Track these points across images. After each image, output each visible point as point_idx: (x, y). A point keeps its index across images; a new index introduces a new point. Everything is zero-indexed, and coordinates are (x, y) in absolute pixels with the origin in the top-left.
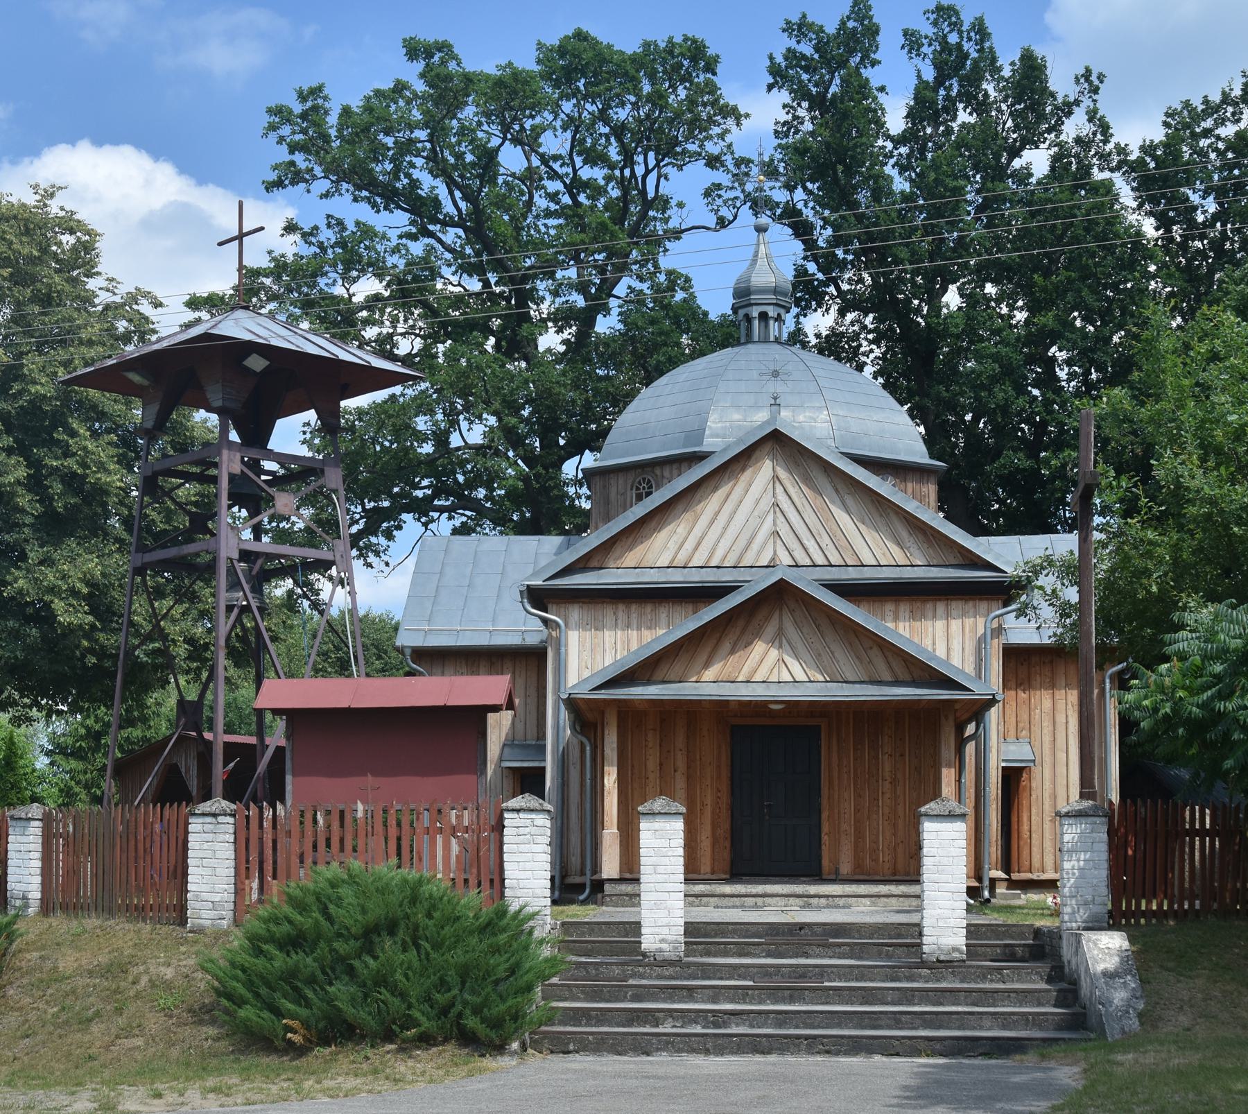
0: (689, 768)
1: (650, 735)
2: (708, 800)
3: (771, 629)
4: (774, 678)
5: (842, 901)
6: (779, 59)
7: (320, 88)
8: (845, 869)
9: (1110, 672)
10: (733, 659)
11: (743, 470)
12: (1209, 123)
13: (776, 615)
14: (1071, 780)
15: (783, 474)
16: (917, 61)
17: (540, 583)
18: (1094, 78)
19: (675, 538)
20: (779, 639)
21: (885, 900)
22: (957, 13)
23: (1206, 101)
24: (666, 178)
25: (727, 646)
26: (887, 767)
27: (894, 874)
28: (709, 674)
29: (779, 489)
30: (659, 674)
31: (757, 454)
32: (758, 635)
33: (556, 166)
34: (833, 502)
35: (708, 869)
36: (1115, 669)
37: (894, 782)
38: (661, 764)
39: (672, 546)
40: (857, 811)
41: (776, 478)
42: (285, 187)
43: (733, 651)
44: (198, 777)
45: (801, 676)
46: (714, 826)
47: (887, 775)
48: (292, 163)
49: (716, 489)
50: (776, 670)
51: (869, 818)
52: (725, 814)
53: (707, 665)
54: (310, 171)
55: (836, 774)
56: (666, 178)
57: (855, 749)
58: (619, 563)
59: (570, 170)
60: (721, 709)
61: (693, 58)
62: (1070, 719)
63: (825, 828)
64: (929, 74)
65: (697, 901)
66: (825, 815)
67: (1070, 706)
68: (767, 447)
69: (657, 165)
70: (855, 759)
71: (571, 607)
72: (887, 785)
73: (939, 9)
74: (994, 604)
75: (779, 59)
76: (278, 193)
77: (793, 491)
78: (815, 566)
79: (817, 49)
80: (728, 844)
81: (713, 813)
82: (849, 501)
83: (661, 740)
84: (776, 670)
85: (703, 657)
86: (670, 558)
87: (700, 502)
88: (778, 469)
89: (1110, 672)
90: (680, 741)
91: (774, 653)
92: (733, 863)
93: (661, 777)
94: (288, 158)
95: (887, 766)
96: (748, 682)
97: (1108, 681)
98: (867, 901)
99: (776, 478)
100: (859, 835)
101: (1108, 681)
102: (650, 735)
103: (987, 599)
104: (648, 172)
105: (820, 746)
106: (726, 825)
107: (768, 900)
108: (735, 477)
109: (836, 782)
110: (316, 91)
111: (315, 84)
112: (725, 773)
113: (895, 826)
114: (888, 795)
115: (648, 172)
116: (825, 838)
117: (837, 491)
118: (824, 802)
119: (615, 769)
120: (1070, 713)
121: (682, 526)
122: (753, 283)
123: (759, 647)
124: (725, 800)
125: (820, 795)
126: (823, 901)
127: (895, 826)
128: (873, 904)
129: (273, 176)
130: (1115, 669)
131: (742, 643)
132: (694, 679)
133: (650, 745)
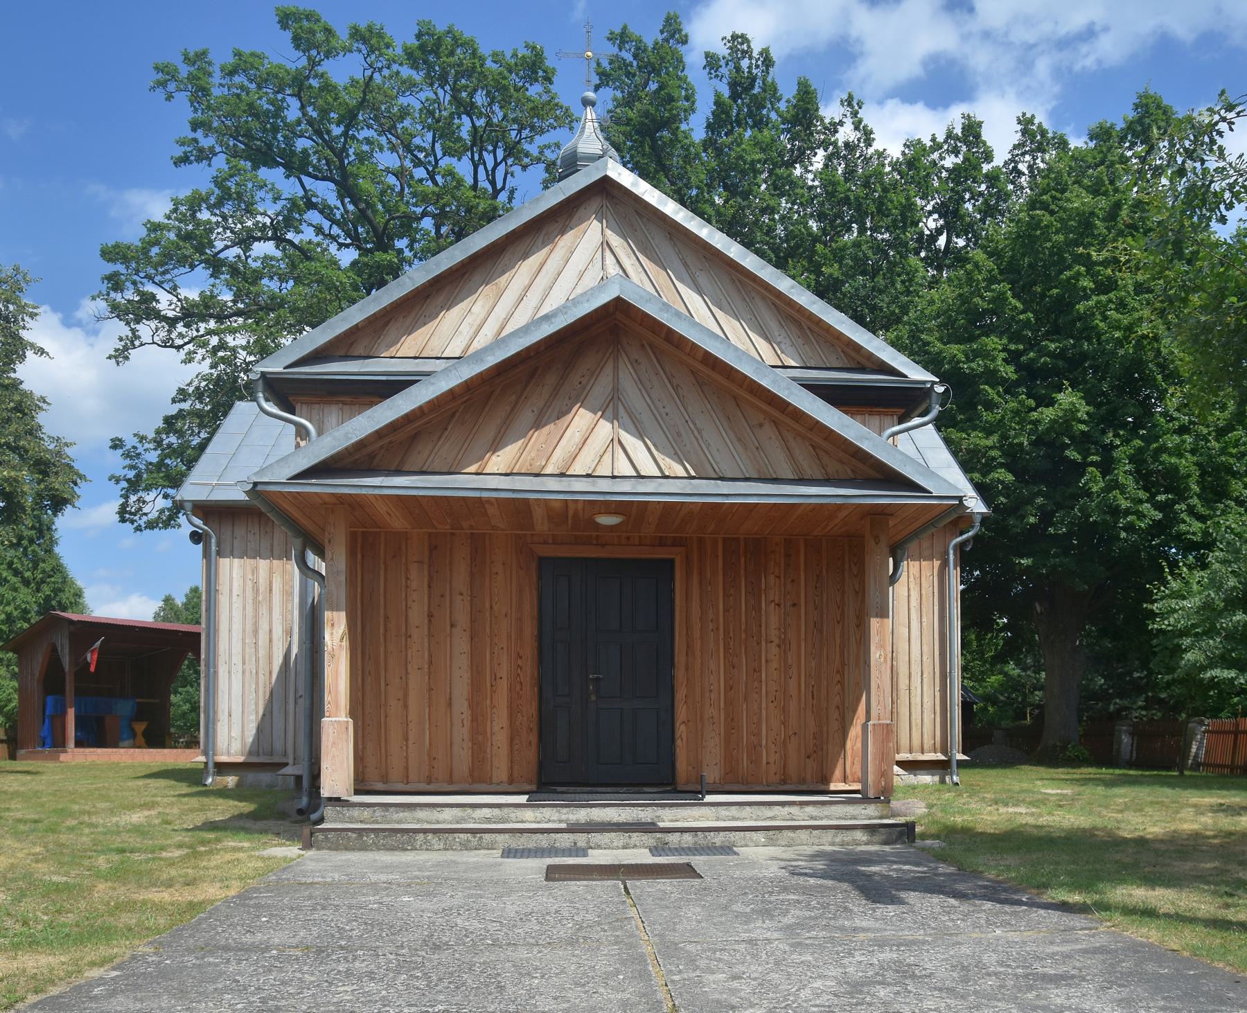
0: (473, 621)
1: (414, 569)
2: (503, 671)
3: (601, 387)
4: (604, 470)
5: (718, 839)
6: (605, 64)
7: (204, 53)
8: (712, 774)
9: (954, 542)
10: (539, 437)
11: (563, 232)
12: (935, 156)
13: (610, 365)
14: (913, 656)
15: (615, 240)
16: (715, 82)
17: (280, 370)
18: (855, 103)
19: (469, 319)
20: (611, 408)
21: (790, 834)
22: (748, 41)
23: (933, 139)
24: (512, 175)
25: (527, 415)
26: (774, 621)
27: (784, 782)
28: (499, 461)
29: (609, 259)
30: (415, 460)
31: (581, 212)
32: (580, 398)
33: (421, 156)
34: (682, 280)
35: (504, 777)
36: (959, 539)
37: (783, 644)
38: (430, 616)
39: (466, 330)
40: (729, 687)
41: (606, 245)
42: (191, 163)
43: (538, 424)
44: (70, 654)
45: (649, 468)
46: (513, 711)
47: (773, 633)
48: (195, 140)
49: (525, 256)
50: (608, 457)
51: (746, 698)
52: (529, 692)
53: (495, 446)
54: (212, 149)
55: (697, 634)
56: (512, 175)
57: (726, 596)
58: (392, 351)
59: (432, 159)
60: (519, 510)
61: (534, 67)
62: (912, 593)
63: (681, 713)
64: (726, 92)
65: (474, 840)
66: (680, 694)
67: (911, 579)
68: (595, 204)
69: (504, 159)
70: (726, 610)
71: (327, 409)
72: (774, 650)
73: (734, 37)
74: (888, 420)
75: (605, 64)
76: (185, 168)
77: (628, 262)
78: (640, 477)
79: (635, 56)
80: (534, 738)
81: (510, 689)
82: (703, 279)
83: (431, 577)
84: (608, 457)
85: (489, 433)
86: (463, 346)
87: (504, 272)
88: (608, 232)
89: (954, 542)
90: (461, 578)
91: (605, 429)
92: (541, 765)
93: (430, 635)
94: (192, 135)
95: (773, 619)
96: (562, 475)
97: (951, 552)
98: (760, 837)
99: (606, 245)
100: (732, 722)
101: (951, 552)
102: (414, 569)
103: (879, 414)
104: (496, 165)
105: (673, 591)
106: (530, 709)
107: (596, 838)
108: (549, 240)
109: (697, 645)
110: (202, 55)
111: (199, 49)
112: (530, 629)
113: (784, 710)
114: (775, 664)
115: (496, 165)
116: (681, 730)
117: (686, 265)
118: (680, 673)
119: (343, 614)
120: (912, 586)
121: (479, 303)
122: (580, 150)
123: (581, 418)
124: (529, 670)
125: (672, 665)
126: (688, 839)
127: (784, 710)
128: (771, 843)
129: (179, 152)
130: (959, 539)
131: (553, 411)
132: (473, 469)
133: (414, 585)
